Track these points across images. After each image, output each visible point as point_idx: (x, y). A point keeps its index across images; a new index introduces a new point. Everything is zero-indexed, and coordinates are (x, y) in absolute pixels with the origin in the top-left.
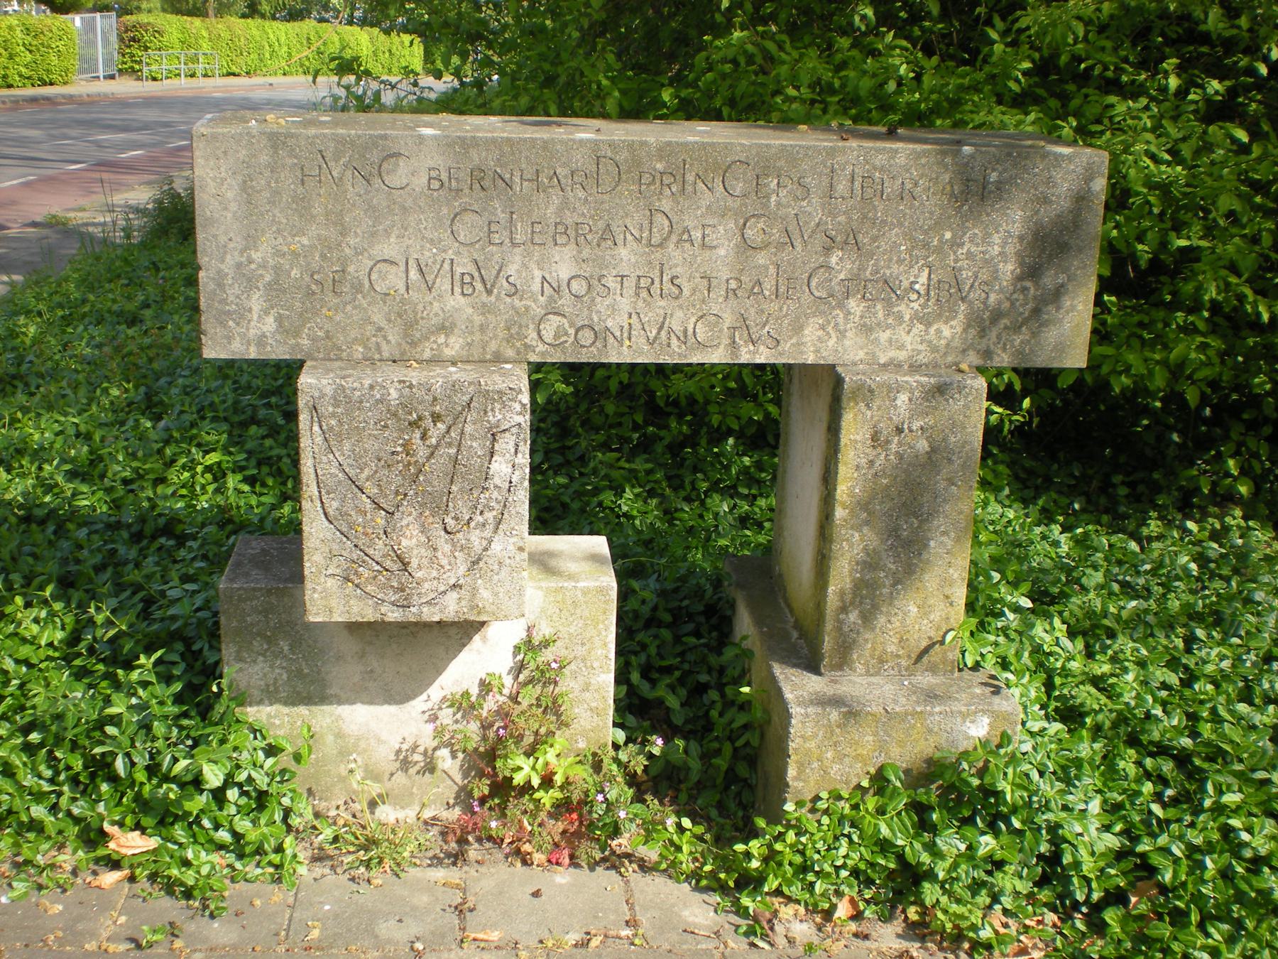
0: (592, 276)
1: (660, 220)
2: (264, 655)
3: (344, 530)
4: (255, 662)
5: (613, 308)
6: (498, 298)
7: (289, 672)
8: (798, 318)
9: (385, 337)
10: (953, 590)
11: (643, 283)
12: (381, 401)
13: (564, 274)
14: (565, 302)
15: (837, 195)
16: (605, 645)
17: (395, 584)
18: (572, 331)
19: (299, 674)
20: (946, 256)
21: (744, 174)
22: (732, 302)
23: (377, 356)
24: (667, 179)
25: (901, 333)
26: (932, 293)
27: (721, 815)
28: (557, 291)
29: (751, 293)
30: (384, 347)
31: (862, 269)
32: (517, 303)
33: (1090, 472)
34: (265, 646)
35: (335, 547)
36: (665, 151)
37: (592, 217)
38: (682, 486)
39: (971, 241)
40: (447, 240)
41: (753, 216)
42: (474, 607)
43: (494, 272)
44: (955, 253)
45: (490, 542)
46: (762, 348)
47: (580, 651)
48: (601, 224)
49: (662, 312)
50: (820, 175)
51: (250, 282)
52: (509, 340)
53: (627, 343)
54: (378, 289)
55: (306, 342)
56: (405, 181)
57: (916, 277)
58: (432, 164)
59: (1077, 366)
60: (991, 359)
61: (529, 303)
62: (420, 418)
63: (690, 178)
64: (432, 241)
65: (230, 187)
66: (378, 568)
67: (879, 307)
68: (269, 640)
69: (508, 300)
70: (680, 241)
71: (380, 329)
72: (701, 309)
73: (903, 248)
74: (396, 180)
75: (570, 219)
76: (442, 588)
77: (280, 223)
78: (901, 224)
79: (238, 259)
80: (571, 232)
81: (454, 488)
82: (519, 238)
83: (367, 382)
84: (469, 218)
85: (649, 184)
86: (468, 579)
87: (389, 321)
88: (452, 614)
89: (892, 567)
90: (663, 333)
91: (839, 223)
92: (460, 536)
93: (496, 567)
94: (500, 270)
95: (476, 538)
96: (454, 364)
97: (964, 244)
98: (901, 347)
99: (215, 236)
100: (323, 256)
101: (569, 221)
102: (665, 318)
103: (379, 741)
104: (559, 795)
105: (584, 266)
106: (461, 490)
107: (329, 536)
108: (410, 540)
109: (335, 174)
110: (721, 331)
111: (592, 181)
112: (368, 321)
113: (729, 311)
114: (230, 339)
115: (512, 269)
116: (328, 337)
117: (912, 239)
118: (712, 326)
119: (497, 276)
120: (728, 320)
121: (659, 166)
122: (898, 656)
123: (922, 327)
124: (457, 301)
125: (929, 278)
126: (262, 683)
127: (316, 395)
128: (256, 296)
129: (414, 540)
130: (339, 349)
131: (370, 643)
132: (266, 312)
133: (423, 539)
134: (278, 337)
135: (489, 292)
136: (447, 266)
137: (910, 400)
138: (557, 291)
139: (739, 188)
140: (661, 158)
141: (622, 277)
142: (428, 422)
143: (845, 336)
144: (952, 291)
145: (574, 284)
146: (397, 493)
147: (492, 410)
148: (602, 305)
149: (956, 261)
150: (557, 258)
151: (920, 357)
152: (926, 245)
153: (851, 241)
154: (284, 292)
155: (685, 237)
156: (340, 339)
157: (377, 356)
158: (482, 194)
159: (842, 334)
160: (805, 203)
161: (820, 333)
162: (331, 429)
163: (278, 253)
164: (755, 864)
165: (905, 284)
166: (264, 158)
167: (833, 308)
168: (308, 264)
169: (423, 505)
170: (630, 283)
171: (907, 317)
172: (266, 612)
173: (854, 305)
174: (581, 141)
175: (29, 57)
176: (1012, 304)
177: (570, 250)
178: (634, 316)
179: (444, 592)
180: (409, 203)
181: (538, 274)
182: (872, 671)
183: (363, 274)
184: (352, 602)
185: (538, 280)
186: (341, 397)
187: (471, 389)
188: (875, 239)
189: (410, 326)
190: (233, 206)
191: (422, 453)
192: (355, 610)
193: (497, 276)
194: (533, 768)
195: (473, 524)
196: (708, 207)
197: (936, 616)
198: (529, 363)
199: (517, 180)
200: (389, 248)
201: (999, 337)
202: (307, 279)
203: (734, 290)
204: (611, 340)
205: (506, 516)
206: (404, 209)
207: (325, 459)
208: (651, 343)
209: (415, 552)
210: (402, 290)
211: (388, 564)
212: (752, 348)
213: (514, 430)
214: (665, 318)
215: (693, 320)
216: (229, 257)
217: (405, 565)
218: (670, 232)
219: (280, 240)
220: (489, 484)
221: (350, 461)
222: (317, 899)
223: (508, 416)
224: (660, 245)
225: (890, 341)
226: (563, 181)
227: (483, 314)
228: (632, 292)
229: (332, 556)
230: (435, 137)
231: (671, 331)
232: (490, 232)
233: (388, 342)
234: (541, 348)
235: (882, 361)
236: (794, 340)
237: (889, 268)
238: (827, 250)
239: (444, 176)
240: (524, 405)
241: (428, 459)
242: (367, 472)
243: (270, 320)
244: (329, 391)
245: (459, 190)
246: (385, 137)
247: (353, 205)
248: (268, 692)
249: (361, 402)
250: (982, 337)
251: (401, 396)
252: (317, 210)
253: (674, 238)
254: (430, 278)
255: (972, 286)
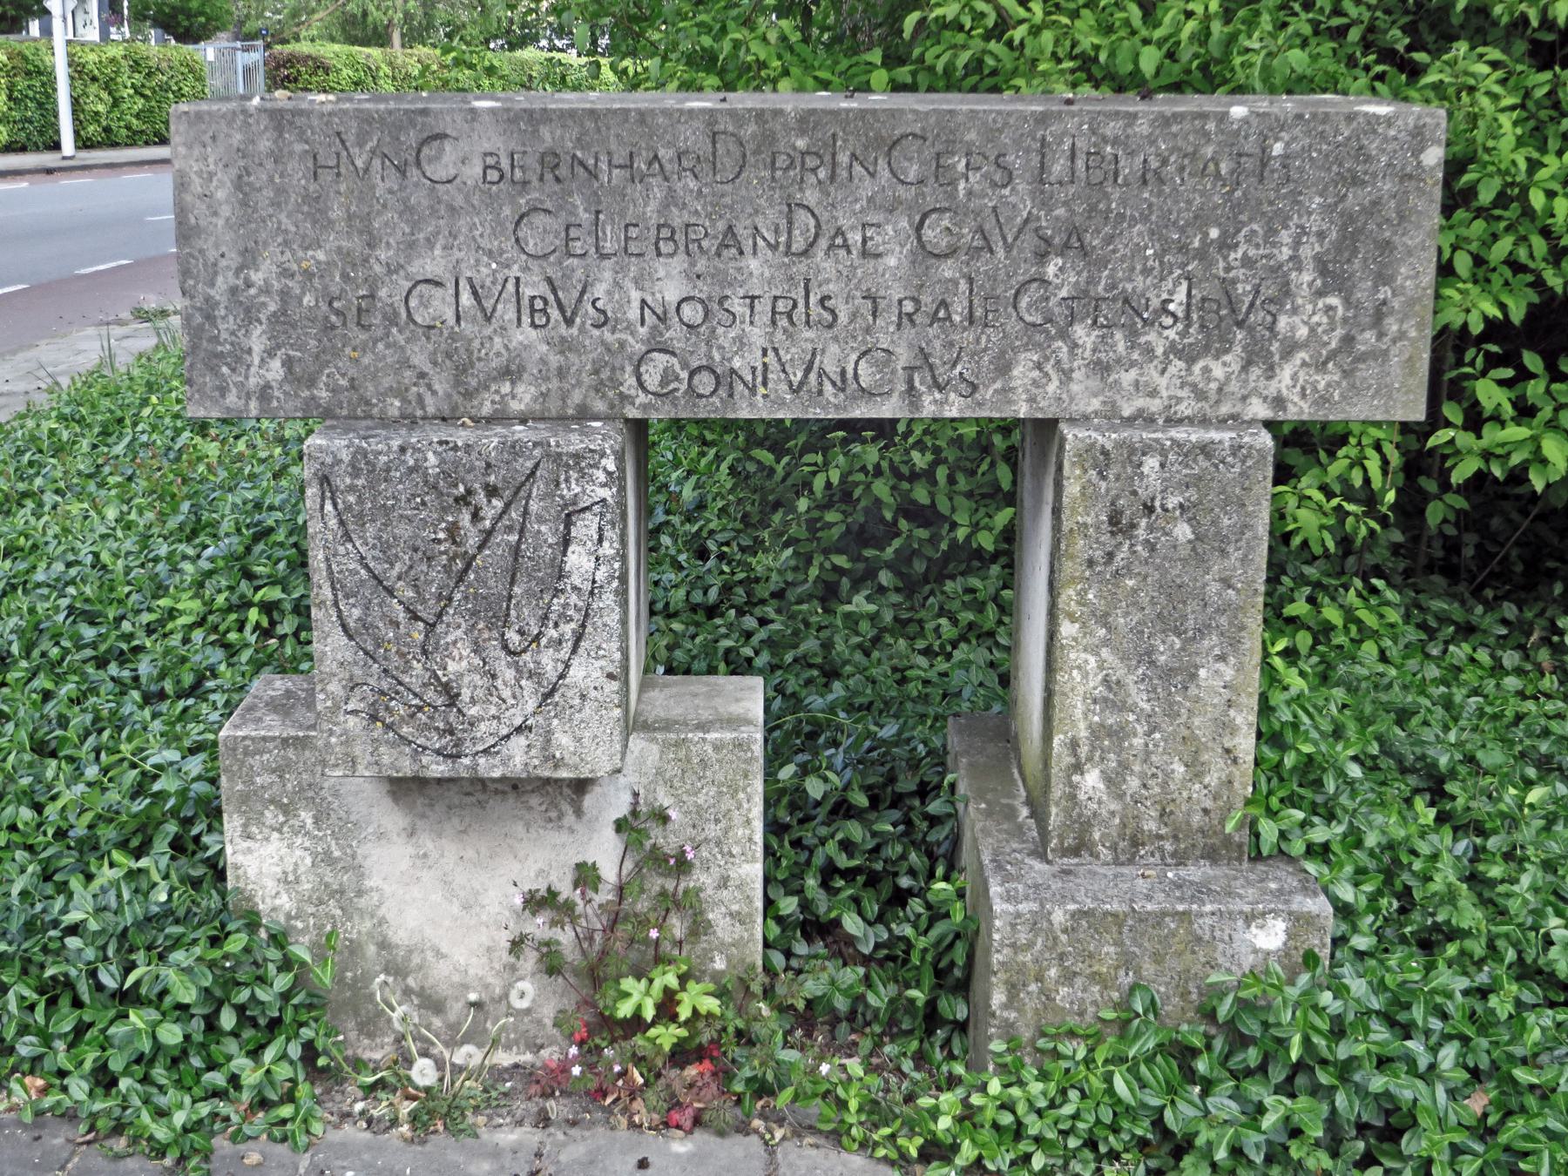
0: (710, 298)
1: (802, 217)
2: (280, 831)
3: (370, 648)
4: (267, 839)
5: (741, 342)
6: (582, 330)
7: (315, 855)
8: (1003, 353)
9: (429, 387)
10: (1236, 741)
11: (781, 306)
12: (412, 470)
13: (672, 294)
14: (674, 334)
15: (1053, 179)
16: (748, 822)
17: (441, 725)
18: (684, 375)
19: (328, 859)
20: (1212, 264)
21: (920, 152)
22: (909, 332)
23: (419, 413)
24: (811, 162)
25: (1152, 372)
26: (1195, 316)
27: (917, 1068)
28: (662, 319)
29: (934, 318)
30: (429, 400)
31: (1092, 281)
32: (608, 336)
33: (1529, 615)
34: (281, 819)
35: (358, 672)
36: (807, 122)
37: (709, 216)
38: (922, 633)
39: (1248, 240)
40: (511, 251)
41: (934, 210)
42: (549, 758)
43: (576, 294)
44: (1225, 258)
45: (567, 666)
46: (952, 396)
47: (713, 831)
48: (721, 226)
49: (810, 346)
50: (1027, 151)
51: (249, 316)
52: (598, 389)
53: (761, 390)
54: (419, 320)
55: (324, 394)
56: (452, 172)
57: (1171, 293)
58: (487, 147)
59: (1400, 415)
60: (1285, 409)
61: (623, 336)
62: (469, 492)
63: (843, 158)
64: (490, 253)
65: (222, 184)
66: (416, 702)
67: (1118, 335)
68: (286, 810)
69: (596, 332)
70: (831, 247)
71: (422, 375)
72: (864, 342)
73: (1149, 252)
74: (439, 171)
75: (677, 218)
76: (505, 731)
77: (286, 231)
78: (1145, 219)
79: (232, 281)
80: (680, 237)
81: (517, 590)
82: (609, 246)
83: (396, 444)
84: (539, 220)
85: (786, 169)
86: (540, 719)
87: (435, 364)
88: (519, 767)
89: (1146, 706)
90: (813, 377)
91: (1057, 218)
92: (527, 657)
93: (577, 701)
94: (583, 292)
95: (549, 662)
96: (523, 421)
97: (1237, 245)
98: (1153, 393)
99: (201, 251)
100: (345, 277)
101: (677, 222)
102: (814, 354)
103: (439, 955)
104: (683, 1032)
105: (700, 283)
106: (528, 593)
107: (349, 656)
108: (459, 664)
109: (359, 163)
110: (893, 372)
111: (706, 167)
112: (405, 363)
113: (904, 344)
114: (223, 391)
115: (599, 290)
116: (353, 387)
117: (1165, 240)
118: (881, 366)
119: (580, 300)
120: (903, 357)
121: (801, 143)
122: (1160, 837)
123: (1181, 364)
124: (525, 335)
125: (1189, 295)
126: (278, 870)
127: (329, 460)
128: (257, 331)
129: (464, 663)
130: (368, 403)
131: (423, 816)
132: (270, 353)
133: (477, 661)
134: (287, 387)
135: (569, 322)
136: (510, 287)
137: (1162, 465)
138: (662, 319)
139: (913, 173)
140: (802, 132)
141: (753, 298)
142: (481, 497)
143: (1070, 379)
144: (1223, 312)
145: (687, 311)
146: (439, 597)
147: (567, 480)
148: (726, 337)
149: (1228, 269)
150: (661, 274)
151: (1181, 407)
152: (1183, 248)
153: (1073, 243)
154: (294, 326)
155: (839, 241)
156: (370, 390)
157: (419, 413)
158: (557, 188)
159: (1067, 376)
160: (1006, 192)
161: (1036, 374)
162: (349, 508)
163: (285, 273)
164: (944, 1123)
165: (1155, 303)
166: (265, 144)
167: (1053, 339)
168: (326, 287)
169: (474, 613)
170: (763, 307)
171: (1160, 351)
172: (280, 771)
173: (1080, 331)
174: (691, 111)
175: (140, 103)
176: (1312, 330)
177: (679, 263)
178: (770, 353)
179: (508, 737)
180: (459, 201)
181: (636, 296)
182: (1123, 858)
183: (398, 300)
184: (382, 749)
185: (636, 304)
186: (361, 462)
187: (537, 452)
188: (1109, 239)
189: (462, 370)
190: (225, 211)
191: (473, 541)
192: (386, 760)
193: (580, 300)
194: (647, 993)
195: (544, 641)
196: (870, 200)
197: (1212, 779)
198: (627, 420)
199: (604, 166)
200: (432, 264)
201: (1294, 377)
202: (324, 307)
203: (909, 315)
204: (739, 387)
205: (589, 629)
206: (452, 209)
207: (341, 550)
208: (795, 391)
209: (466, 679)
210: (451, 321)
211: (430, 695)
212: (938, 396)
213: (596, 509)
214: (814, 354)
215: (854, 357)
216: (220, 279)
217: (453, 698)
218: (817, 236)
219: (288, 255)
220: (566, 584)
221: (377, 553)
222: (339, 1163)
223: (589, 488)
224: (805, 253)
225: (1137, 384)
226: (668, 167)
227: (562, 352)
228: (767, 318)
229: (353, 685)
230: (492, 111)
231: (822, 373)
232: (568, 239)
233: (434, 393)
234: (642, 398)
235: (1126, 413)
236: (998, 385)
237: (1131, 280)
238: (1042, 257)
239: (505, 164)
240: (609, 474)
241: (481, 548)
242: (398, 567)
243: (276, 364)
244: (345, 456)
245: (525, 183)
246: (424, 112)
247: (385, 206)
248: (286, 882)
249: (388, 470)
250: (1269, 378)
251: (443, 462)
252: (336, 213)
253: (823, 243)
254: (488, 304)
255: (1252, 305)
